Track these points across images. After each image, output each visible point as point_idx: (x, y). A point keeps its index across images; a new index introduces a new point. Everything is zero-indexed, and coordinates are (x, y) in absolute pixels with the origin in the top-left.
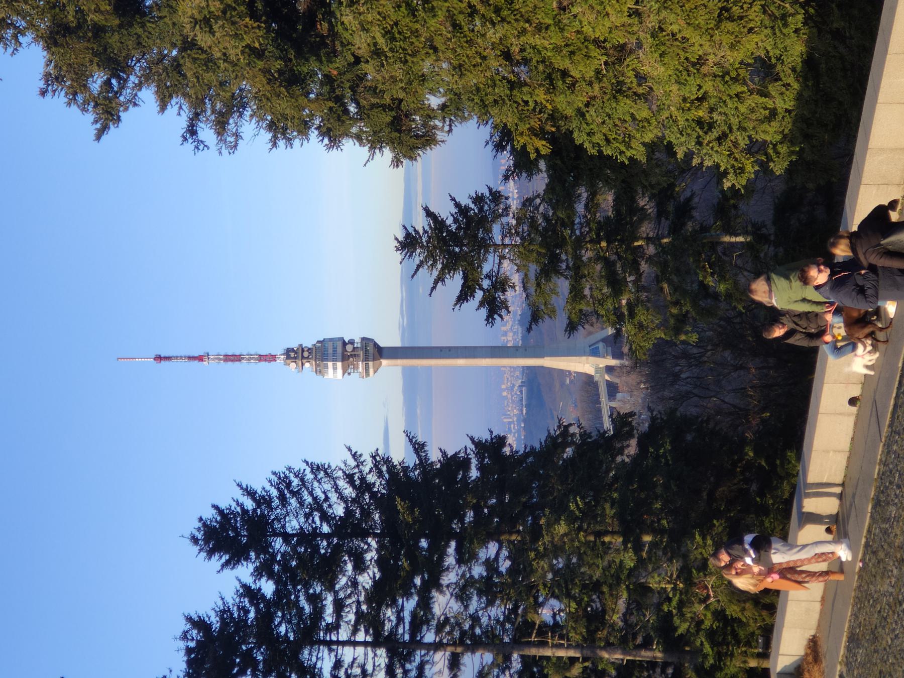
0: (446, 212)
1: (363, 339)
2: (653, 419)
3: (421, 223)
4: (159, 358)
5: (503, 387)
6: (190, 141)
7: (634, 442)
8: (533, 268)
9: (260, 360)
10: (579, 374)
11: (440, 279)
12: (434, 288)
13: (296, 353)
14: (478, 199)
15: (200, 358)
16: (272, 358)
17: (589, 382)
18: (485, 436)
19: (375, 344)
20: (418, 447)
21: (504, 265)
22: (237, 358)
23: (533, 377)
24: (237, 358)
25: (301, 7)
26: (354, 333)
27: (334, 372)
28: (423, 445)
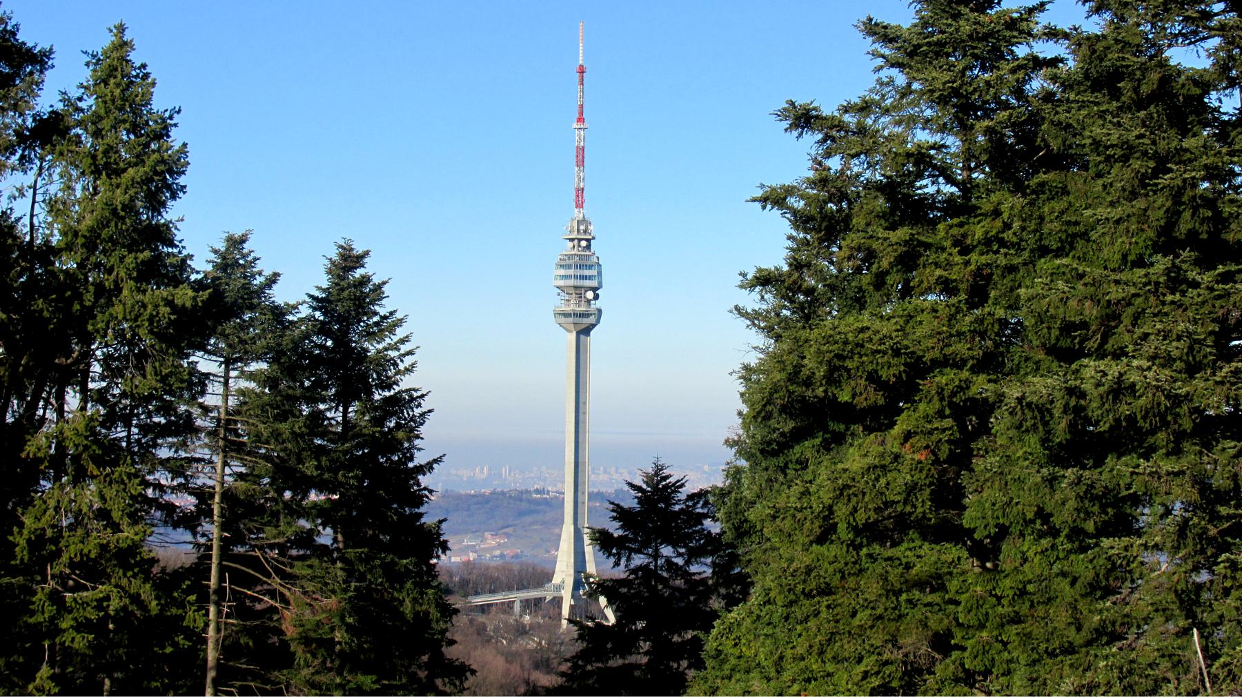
1: (600, 311)
4: (582, 71)
5: (544, 468)
9: (577, 190)
10: (554, 562)
13: (585, 232)
15: (581, 119)
17: (543, 577)
19: (594, 326)
20: (429, 466)
22: (580, 162)
24: (580, 162)
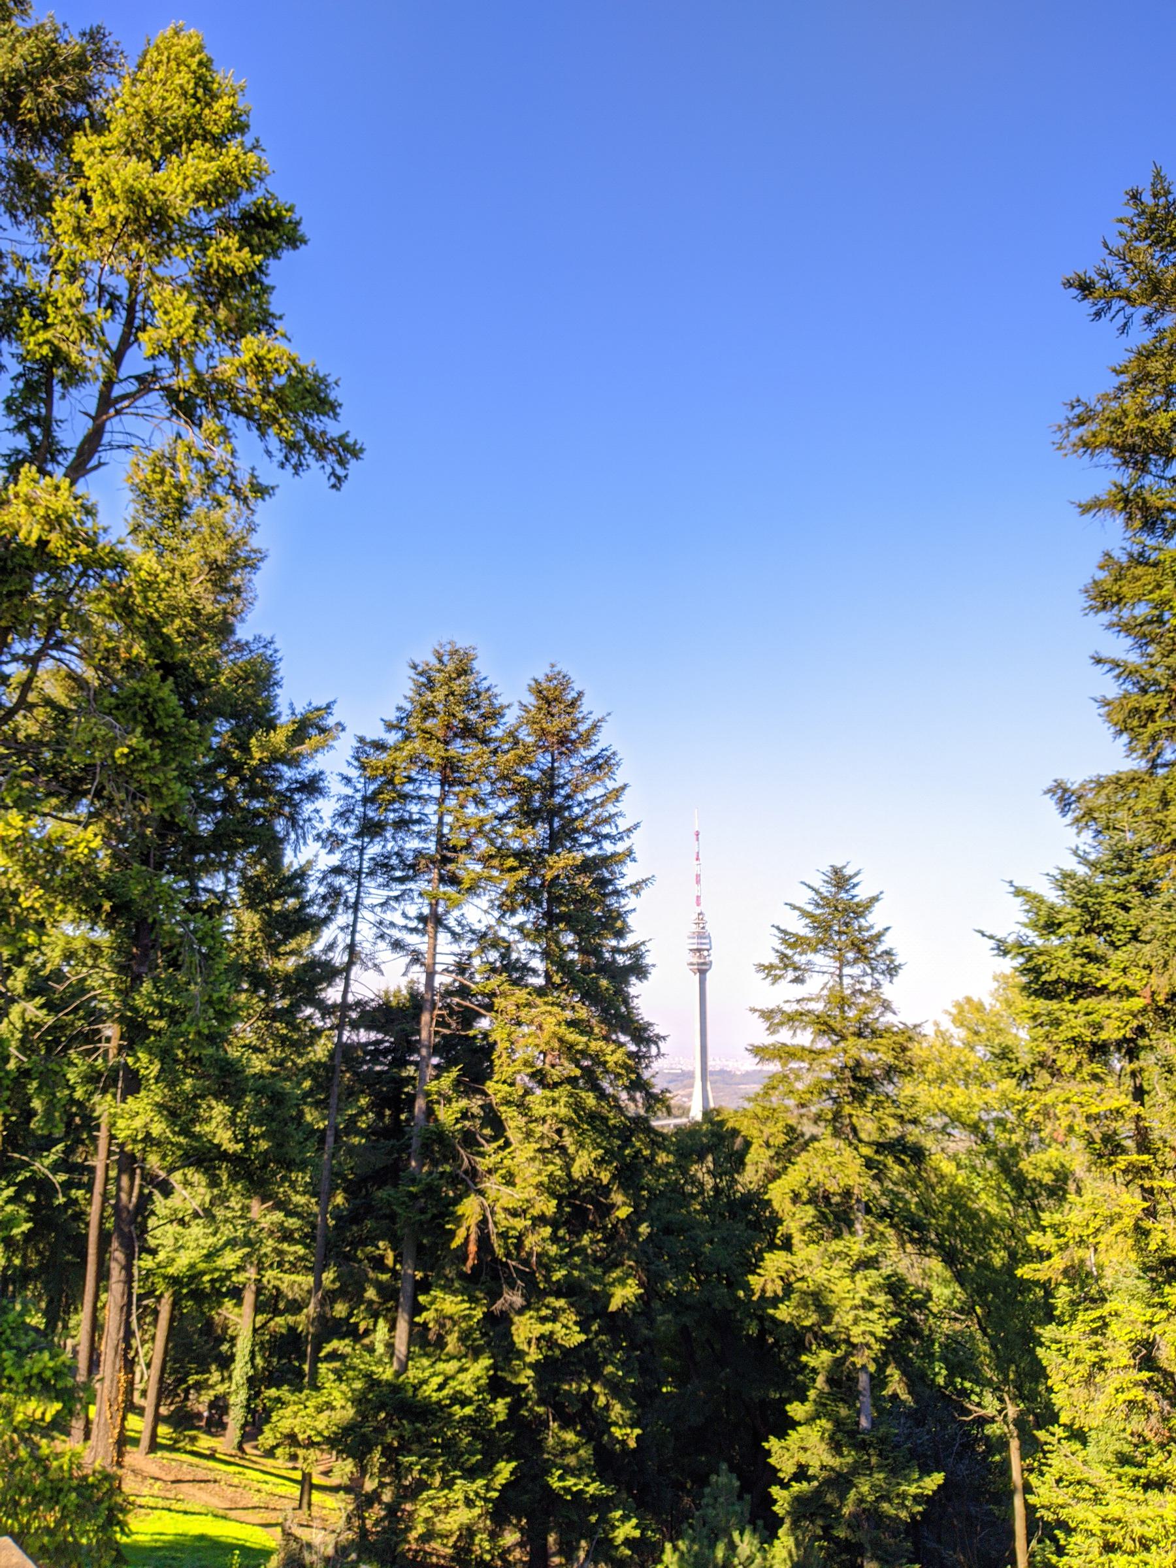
0: (875, 919)
3: (862, 893)
8: (818, 1007)
11: (805, 914)
12: (795, 908)
16: (698, 904)
18: (648, 960)
21: (821, 974)
22: (698, 882)
23: (691, 1075)
24: (698, 882)
26: (714, 957)
28: (638, 893)
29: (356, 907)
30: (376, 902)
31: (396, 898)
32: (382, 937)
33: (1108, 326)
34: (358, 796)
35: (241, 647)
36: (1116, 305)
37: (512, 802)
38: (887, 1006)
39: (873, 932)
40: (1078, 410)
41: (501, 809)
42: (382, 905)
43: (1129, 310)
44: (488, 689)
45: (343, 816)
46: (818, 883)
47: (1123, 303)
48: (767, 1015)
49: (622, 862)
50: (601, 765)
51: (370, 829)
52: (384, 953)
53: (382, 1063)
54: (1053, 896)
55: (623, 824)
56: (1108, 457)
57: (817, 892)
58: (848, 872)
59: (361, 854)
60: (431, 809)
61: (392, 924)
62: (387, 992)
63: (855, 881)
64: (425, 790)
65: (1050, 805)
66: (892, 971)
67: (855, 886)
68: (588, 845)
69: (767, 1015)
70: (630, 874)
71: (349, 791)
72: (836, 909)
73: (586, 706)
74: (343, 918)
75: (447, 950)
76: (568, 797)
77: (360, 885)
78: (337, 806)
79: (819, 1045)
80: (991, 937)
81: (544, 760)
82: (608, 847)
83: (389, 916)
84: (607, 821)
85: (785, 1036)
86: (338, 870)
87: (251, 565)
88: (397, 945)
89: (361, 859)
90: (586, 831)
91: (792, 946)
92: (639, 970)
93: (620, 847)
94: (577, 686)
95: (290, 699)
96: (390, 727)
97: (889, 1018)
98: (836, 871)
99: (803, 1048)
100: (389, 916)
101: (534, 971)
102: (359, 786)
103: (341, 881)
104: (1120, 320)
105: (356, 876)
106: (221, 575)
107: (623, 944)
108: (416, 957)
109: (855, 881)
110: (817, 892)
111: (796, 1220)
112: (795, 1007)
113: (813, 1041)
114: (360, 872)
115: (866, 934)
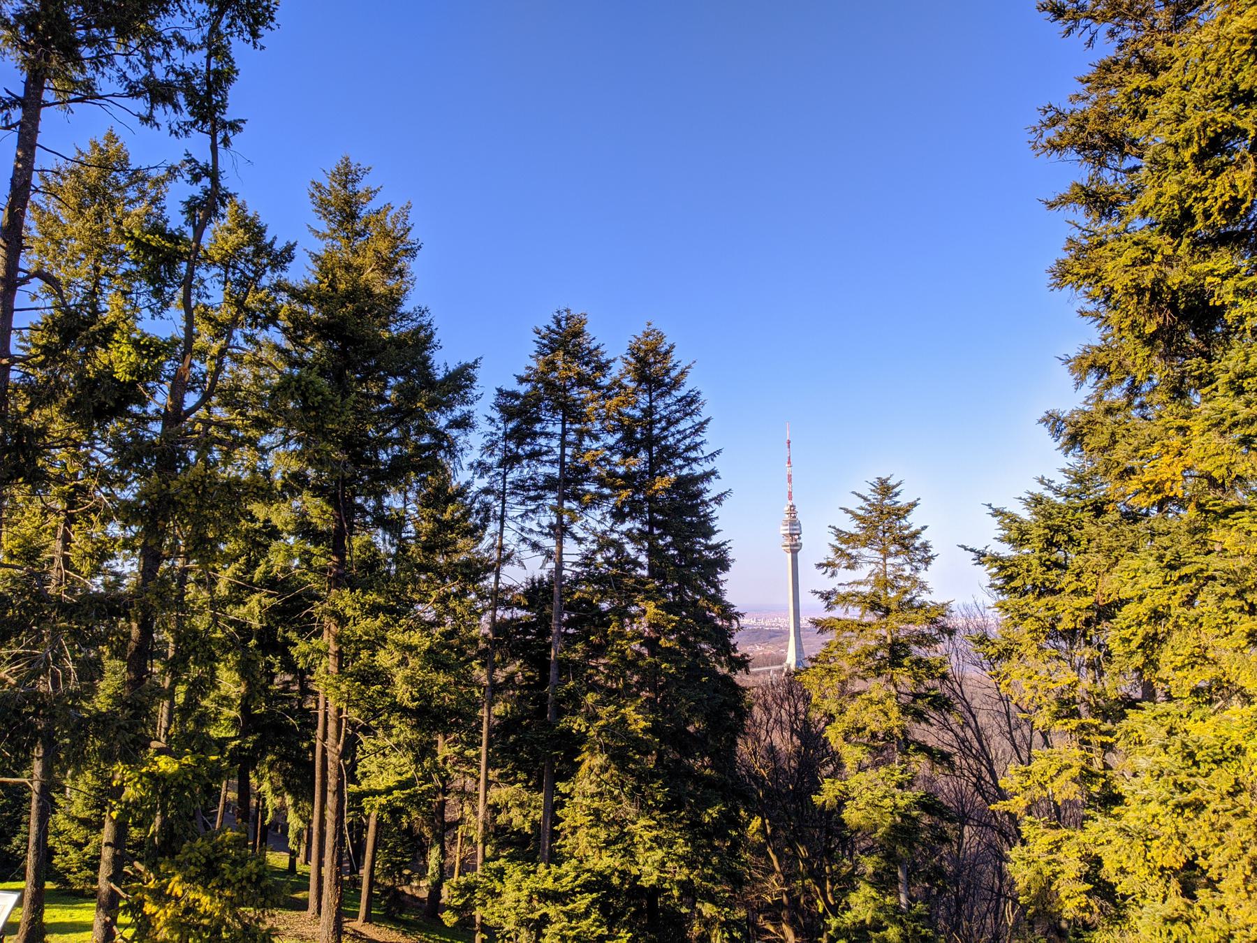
0: (914, 520)
2: (744, 689)
3: (903, 500)
6: (1044, 119)
7: (725, 671)
8: (866, 589)
11: (856, 516)
12: (847, 511)
14: (925, 547)
16: (790, 498)
22: (790, 481)
23: (787, 633)
24: (790, 481)
25: (625, 935)
26: (804, 540)
27: (784, 530)
29: (502, 519)
30: (516, 514)
31: (533, 511)
32: (524, 540)
33: (1079, 38)
34: (500, 433)
35: (404, 316)
36: (1083, 23)
37: (618, 436)
38: (923, 587)
39: (913, 529)
40: (1050, 114)
41: (611, 440)
42: (522, 516)
43: (1094, 26)
44: (596, 349)
45: (489, 448)
46: (866, 492)
47: (1089, 21)
48: (826, 596)
49: (708, 480)
50: (689, 403)
51: (510, 460)
52: (525, 551)
53: (530, 634)
54: (1025, 514)
55: (707, 449)
56: (1071, 155)
57: (865, 499)
58: (892, 482)
59: (504, 477)
60: (555, 443)
61: (531, 531)
62: (532, 580)
63: (896, 490)
64: (550, 429)
65: (1044, 431)
66: (927, 561)
67: (897, 494)
68: (681, 467)
69: (826, 596)
70: (713, 488)
71: (493, 430)
72: (882, 512)
73: (675, 357)
74: (493, 527)
75: (572, 551)
76: (663, 429)
77: (504, 502)
78: (484, 441)
79: (866, 620)
80: (972, 550)
81: (644, 400)
82: (698, 469)
83: (528, 524)
84: (695, 447)
85: (838, 612)
86: (487, 491)
87: (411, 252)
88: (535, 546)
89: (505, 482)
90: (679, 456)
91: (845, 542)
92: (723, 564)
93: (707, 467)
94: (668, 341)
95: (443, 361)
96: (521, 380)
97: (925, 597)
98: (883, 482)
99: (853, 622)
100: (528, 524)
101: (641, 565)
102: (501, 425)
103: (490, 498)
104: (1087, 36)
105: (502, 496)
106: (388, 266)
107: (710, 543)
108: (549, 555)
109: (896, 490)
110: (865, 499)
111: (851, 754)
112: (848, 589)
113: (862, 616)
114: (504, 493)
115: (906, 532)
